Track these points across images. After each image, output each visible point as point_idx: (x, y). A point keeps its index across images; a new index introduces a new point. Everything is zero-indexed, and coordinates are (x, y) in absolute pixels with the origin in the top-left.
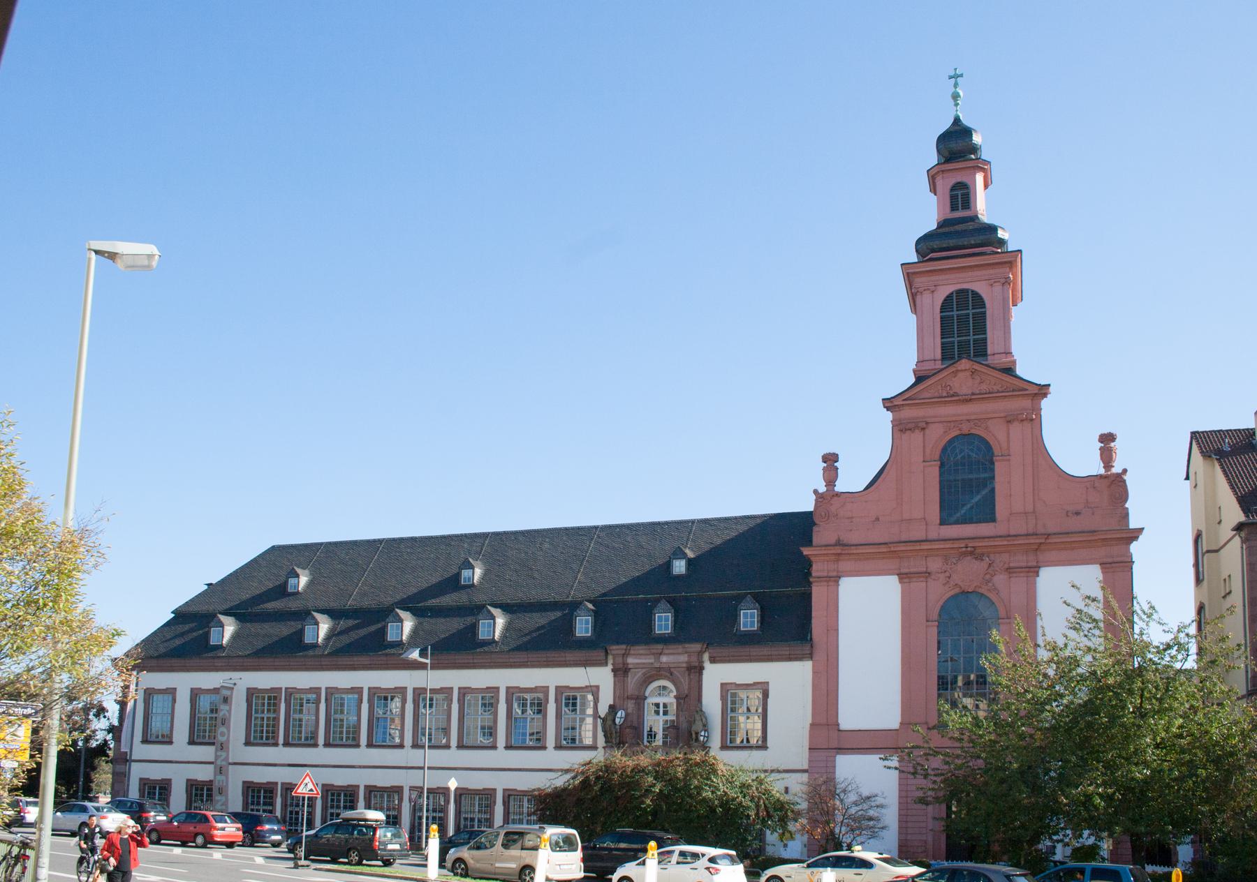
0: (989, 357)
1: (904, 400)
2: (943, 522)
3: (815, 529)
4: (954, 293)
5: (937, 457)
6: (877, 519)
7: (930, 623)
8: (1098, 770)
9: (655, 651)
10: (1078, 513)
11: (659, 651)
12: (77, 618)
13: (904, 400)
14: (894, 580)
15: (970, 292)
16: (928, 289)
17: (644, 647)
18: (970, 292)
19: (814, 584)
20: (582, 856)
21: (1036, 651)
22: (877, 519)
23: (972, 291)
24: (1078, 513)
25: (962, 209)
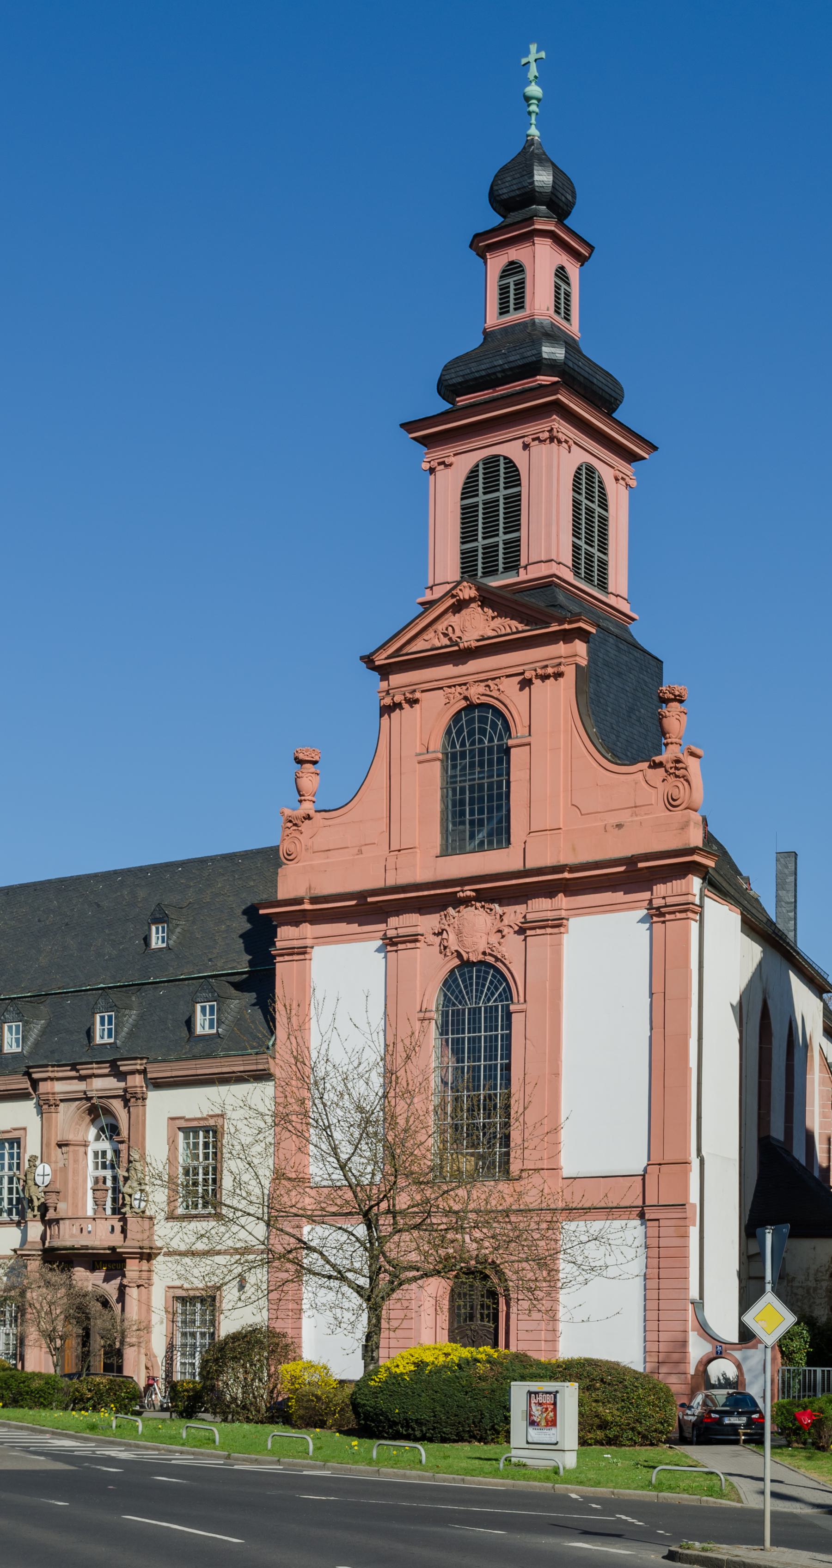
0: (522, 571)
1: (386, 658)
2: (445, 852)
13: (386, 658)
15: (502, 461)
18: (502, 461)
22: (360, 852)
23: (505, 458)
24: (619, 826)
25: (515, 309)
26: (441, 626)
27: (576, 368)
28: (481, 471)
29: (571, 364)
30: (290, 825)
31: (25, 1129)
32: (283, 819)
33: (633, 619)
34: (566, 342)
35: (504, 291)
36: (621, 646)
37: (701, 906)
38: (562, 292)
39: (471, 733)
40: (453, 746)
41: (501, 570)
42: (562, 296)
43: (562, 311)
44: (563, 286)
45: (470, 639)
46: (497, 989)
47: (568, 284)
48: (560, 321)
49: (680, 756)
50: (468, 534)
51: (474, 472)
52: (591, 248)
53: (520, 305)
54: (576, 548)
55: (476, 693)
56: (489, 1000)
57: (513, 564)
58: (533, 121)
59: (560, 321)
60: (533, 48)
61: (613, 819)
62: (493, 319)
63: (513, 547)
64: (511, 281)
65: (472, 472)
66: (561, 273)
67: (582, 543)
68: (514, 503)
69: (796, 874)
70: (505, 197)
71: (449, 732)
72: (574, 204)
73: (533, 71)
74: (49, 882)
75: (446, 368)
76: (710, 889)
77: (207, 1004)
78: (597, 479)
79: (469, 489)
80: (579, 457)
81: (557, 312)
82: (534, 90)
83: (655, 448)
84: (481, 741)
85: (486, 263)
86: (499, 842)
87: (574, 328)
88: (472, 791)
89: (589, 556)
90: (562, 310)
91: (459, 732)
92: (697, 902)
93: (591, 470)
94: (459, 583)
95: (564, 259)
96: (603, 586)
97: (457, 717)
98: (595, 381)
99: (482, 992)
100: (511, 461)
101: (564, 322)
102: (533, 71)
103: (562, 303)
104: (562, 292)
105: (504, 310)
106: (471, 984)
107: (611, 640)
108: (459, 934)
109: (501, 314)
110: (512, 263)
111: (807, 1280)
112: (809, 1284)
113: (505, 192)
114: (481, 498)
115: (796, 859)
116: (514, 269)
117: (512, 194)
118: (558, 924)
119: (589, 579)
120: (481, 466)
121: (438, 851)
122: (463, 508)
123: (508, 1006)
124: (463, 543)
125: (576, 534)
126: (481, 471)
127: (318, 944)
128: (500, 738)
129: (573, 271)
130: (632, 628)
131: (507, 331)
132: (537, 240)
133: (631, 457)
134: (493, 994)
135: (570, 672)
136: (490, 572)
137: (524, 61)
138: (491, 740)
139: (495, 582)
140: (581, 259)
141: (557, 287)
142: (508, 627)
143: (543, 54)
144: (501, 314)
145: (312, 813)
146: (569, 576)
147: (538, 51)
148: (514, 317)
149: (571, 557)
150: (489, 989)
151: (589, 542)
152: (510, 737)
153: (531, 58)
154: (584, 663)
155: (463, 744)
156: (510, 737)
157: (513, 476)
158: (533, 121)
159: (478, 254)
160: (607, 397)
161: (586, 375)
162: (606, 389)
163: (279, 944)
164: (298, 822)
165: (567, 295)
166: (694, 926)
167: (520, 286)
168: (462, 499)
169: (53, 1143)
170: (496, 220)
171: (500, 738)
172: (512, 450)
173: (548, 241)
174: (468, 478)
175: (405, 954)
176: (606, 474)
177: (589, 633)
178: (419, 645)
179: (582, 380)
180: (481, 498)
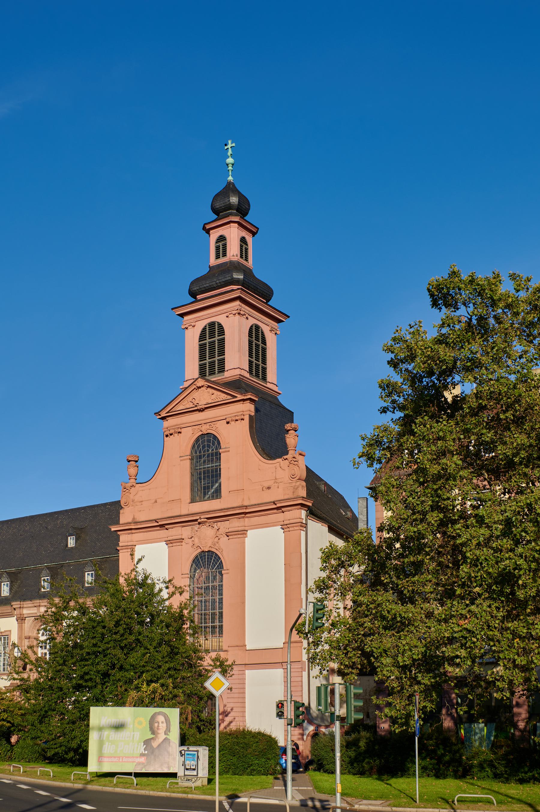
2: (193, 501)
3: (121, 511)
4: (207, 326)
5: (188, 452)
6: (156, 502)
7: (183, 576)
8: (57, 702)
9: (36, 605)
10: (269, 488)
11: (38, 604)
12: (504, 370)
14: (163, 547)
16: (191, 325)
17: (30, 602)
19: (120, 551)
20: (253, 731)
21: (492, 548)
22: (156, 502)
23: (218, 323)
24: (269, 488)
25: (223, 256)
26: (190, 398)
27: (249, 282)
28: (207, 329)
29: (246, 280)
30: (125, 490)
31: (10, 631)
32: (122, 487)
33: (280, 394)
34: (244, 270)
35: (218, 248)
36: (272, 406)
37: (306, 524)
38: (244, 248)
39: (204, 447)
40: (196, 453)
41: (216, 373)
42: (244, 250)
43: (244, 257)
44: (244, 246)
45: (202, 403)
46: (216, 564)
47: (247, 245)
48: (243, 261)
49: (295, 455)
50: (202, 357)
51: (204, 329)
52: (258, 229)
53: (225, 255)
54: (250, 362)
55: (205, 429)
56: (213, 569)
57: (222, 370)
58: (230, 174)
59: (243, 261)
60: (230, 142)
61: (267, 485)
62: (213, 261)
63: (222, 362)
64: (221, 244)
65: (203, 329)
66: (243, 240)
67: (254, 360)
68: (222, 342)
69: (367, 507)
70: (218, 207)
71: (193, 447)
72: (249, 209)
73: (230, 152)
74: (26, 517)
75: (192, 283)
76: (311, 516)
77: (90, 573)
78: (260, 332)
79: (202, 337)
80: (252, 321)
81: (241, 257)
82: (230, 160)
83: (289, 317)
84: (208, 451)
85: (210, 236)
86: (217, 496)
87: (250, 264)
88: (204, 473)
89: (257, 366)
90: (244, 257)
91: (198, 447)
92: (304, 522)
93: (257, 327)
94: (197, 379)
95: (244, 234)
96: (264, 379)
97: (197, 440)
98: (259, 287)
99: (210, 565)
100: (220, 324)
101: (245, 262)
102: (230, 152)
103: (244, 252)
104: (244, 248)
105: (218, 257)
106: (205, 562)
107: (267, 404)
108: (199, 538)
109: (217, 258)
110: (221, 236)
111: (366, 695)
112: (367, 697)
113: (218, 205)
114: (208, 341)
115: (367, 501)
116: (222, 238)
117: (221, 206)
118: (243, 533)
119: (257, 376)
120: (207, 326)
121: (189, 500)
122: (200, 345)
123: (221, 571)
124: (200, 361)
125: (250, 355)
126: (207, 329)
127: (139, 544)
128: (216, 449)
129: (249, 239)
130: (279, 397)
131: (219, 266)
132: (232, 224)
133: (279, 321)
134: (215, 566)
135: (247, 418)
136: (212, 373)
137: (226, 148)
138: (213, 450)
139: (213, 378)
140: (254, 234)
141: (241, 246)
142: (221, 397)
143: (234, 145)
144: (217, 258)
145: (134, 484)
146: (247, 375)
147: (232, 143)
148: (222, 260)
149: (248, 366)
150: (213, 563)
151: (257, 359)
152: (220, 448)
153: (229, 146)
154: (253, 414)
155: (200, 452)
156: (220, 448)
157: (222, 331)
158: (230, 174)
159: (206, 232)
160: (265, 294)
161: (254, 285)
162: (265, 291)
163: (120, 544)
164: (129, 488)
165: (246, 249)
166: (303, 534)
167: (225, 246)
168: (199, 341)
169: (23, 637)
170: (216, 217)
171: (216, 449)
172: (221, 319)
173: (236, 225)
174: (202, 332)
175: (177, 548)
176: (266, 329)
177: (255, 400)
178: (180, 407)
179: (253, 287)
180: (208, 341)
